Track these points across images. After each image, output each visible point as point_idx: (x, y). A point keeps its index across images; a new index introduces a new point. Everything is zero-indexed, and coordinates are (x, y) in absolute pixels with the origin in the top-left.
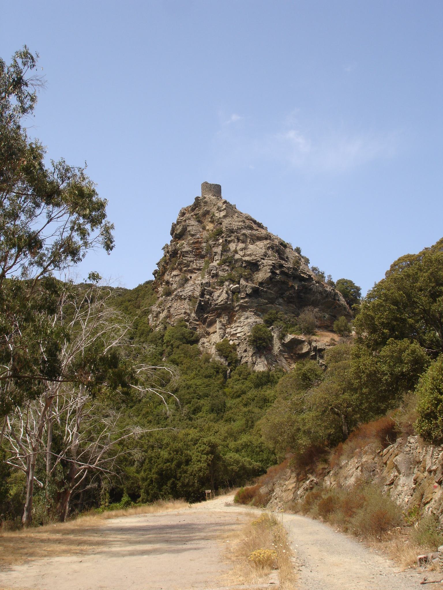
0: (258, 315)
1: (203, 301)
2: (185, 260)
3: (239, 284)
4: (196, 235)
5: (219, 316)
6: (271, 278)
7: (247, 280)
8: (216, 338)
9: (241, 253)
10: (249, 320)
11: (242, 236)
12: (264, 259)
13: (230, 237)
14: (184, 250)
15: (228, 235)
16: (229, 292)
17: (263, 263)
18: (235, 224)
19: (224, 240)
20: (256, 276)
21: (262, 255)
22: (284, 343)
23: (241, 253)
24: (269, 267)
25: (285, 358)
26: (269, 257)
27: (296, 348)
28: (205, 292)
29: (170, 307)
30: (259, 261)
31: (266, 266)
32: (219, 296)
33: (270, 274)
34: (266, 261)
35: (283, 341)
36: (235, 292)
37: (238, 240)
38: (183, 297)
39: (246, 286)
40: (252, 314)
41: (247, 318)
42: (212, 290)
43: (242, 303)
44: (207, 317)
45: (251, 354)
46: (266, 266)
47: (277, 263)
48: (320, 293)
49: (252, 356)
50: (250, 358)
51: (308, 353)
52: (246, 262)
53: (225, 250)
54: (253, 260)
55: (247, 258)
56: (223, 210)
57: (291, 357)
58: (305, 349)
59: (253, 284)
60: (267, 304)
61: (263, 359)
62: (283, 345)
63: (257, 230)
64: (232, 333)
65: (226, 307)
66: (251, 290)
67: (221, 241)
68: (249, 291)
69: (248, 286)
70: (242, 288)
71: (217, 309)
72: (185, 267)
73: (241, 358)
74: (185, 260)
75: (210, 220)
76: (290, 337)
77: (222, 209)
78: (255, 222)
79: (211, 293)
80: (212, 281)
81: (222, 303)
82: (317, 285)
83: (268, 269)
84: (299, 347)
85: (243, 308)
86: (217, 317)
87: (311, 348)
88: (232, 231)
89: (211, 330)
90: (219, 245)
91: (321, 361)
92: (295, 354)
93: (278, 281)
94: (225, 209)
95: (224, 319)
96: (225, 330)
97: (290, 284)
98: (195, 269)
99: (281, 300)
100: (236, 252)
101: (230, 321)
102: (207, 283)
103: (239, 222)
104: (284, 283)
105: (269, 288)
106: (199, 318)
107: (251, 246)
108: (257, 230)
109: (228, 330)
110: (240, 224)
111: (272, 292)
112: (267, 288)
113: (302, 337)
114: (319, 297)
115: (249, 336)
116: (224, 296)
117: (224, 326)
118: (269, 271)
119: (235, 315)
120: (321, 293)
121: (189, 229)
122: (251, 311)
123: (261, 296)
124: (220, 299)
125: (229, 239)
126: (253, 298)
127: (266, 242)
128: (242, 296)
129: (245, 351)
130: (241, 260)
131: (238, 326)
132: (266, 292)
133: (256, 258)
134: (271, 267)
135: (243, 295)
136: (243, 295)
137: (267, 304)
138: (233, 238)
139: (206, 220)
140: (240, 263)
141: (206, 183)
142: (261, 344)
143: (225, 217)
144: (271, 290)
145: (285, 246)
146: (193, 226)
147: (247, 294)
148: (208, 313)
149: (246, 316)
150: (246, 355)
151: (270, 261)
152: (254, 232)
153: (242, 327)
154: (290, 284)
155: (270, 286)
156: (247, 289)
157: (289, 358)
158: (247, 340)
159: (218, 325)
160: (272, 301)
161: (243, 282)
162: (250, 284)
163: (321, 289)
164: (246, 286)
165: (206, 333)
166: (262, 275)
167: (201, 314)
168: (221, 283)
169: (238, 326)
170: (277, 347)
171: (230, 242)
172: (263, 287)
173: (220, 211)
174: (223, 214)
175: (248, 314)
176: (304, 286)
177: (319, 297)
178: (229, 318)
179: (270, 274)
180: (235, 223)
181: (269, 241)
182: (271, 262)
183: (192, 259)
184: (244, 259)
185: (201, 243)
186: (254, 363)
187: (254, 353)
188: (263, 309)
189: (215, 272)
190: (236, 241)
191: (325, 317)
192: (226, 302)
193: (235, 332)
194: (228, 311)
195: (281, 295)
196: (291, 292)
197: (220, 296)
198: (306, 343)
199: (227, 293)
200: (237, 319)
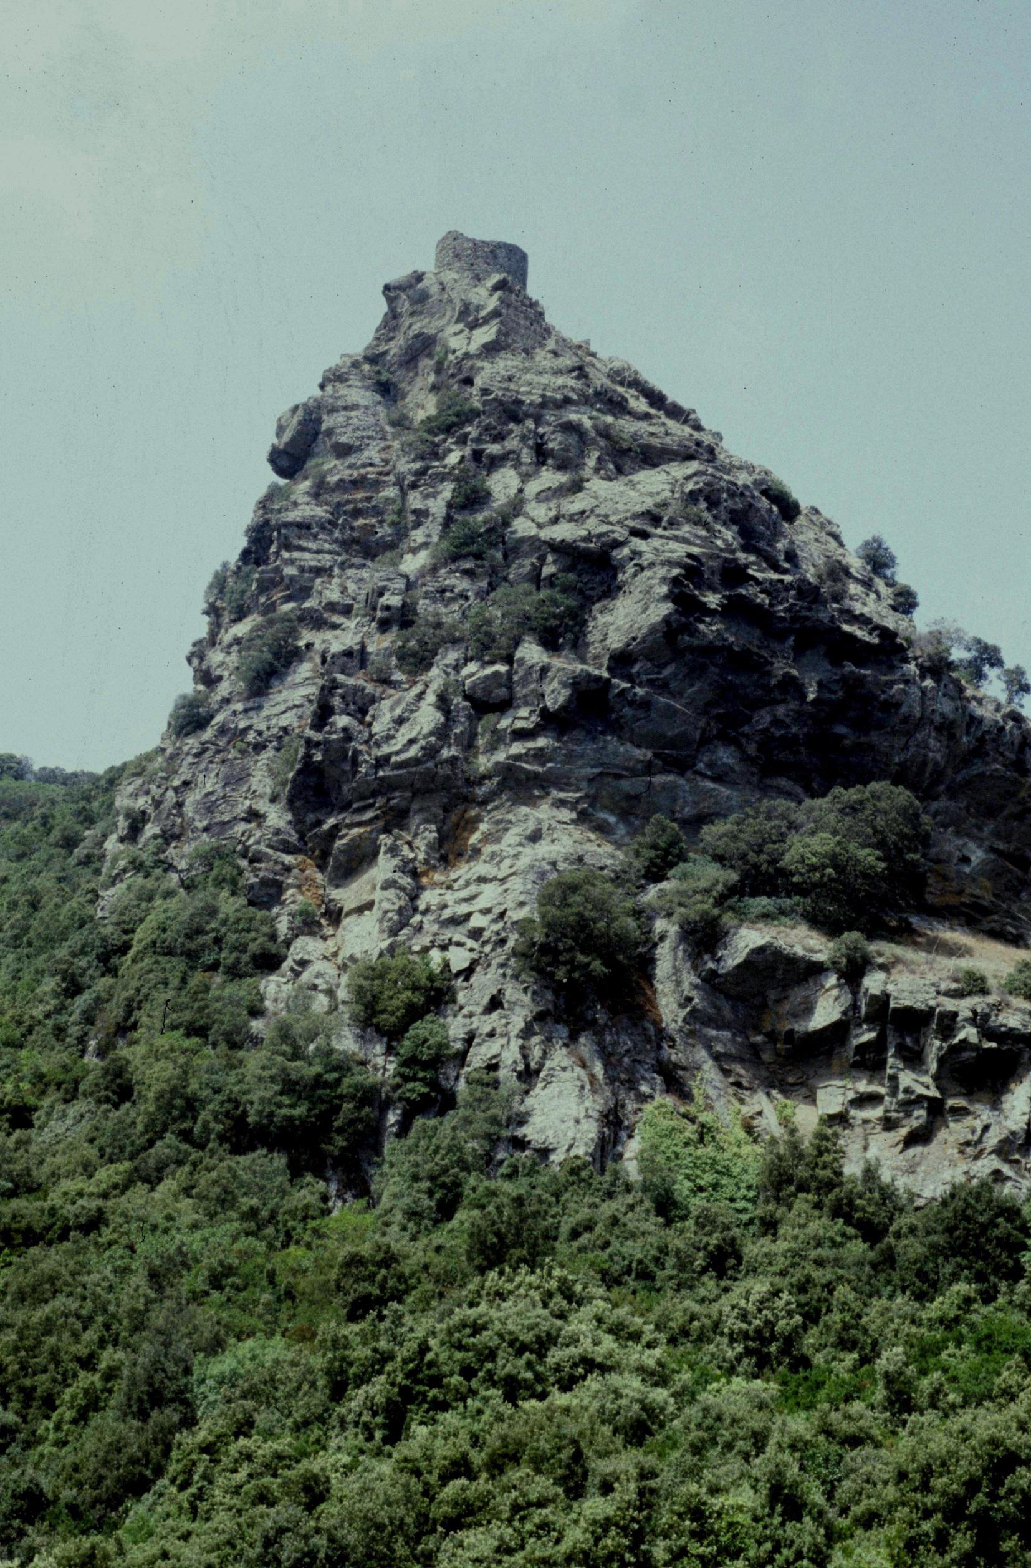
0: (602, 829)
1: (318, 744)
2: (292, 562)
3: (509, 659)
4: (359, 449)
5: (395, 820)
6: (669, 630)
7: (550, 643)
8: (362, 937)
9: (541, 512)
10: (544, 849)
11: (559, 437)
12: (644, 535)
13: (499, 438)
14: (293, 516)
15: (488, 428)
16: (458, 700)
17: (636, 554)
18: (537, 379)
19: (468, 451)
20: (602, 619)
21: (636, 516)
22: (713, 973)
23: (541, 512)
24: (662, 572)
25: (717, 1057)
26: (672, 523)
27: (778, 1001)
28: (336, 701)
29: (186, 784)
30: (618, 544)
31: (652, 565)
32: (400, 721)
33: (667, 608)
34: (655, 543)
35: (711, 965)
36: (487, 703)
37: (541, 454)
38: (251, 737)
39: (544, 670)
40: (566, 814)
41: (535, 837)
42: (370, 688)
43: (518, 757)
44: (336, 827)
45: (518, 1023)
46: (652, 565)
47: (711, 557)
48: (939, 729)
49: (527, 1033)
50: (515, 1044)
51: (838, 1031)
52: (560, 548)
53: (472, 498)
54: (588, 538)
55: (563, 532)
56: (486, 321)
57: (752, 1056)
58: (826, 1011)
59: (583, 661)
60: (648, 769)
61: (586, 1045)
62: (711, 981)
63: (647, 416)
64: (446, 914)
65: (432, 776)
66: (566, 693)
67: (453, 459)
68: (556, 695)
69: (550, 674)
70: (524, 681)
71: (385, 787)
72: (288, 599)
73: (469, 1040)
74: (292, 562)
75: (432, 378)
76: (747, 939)
77: (483, 313)
78: (637, 384)
79: (362, 708)
80: (380, 644)
81: (413, 751)
82: (929, 683)
83: (656, 582)
84: (798, 994)
85: (519, 784)
86: (387, 830)
87: (855, 1006)
88: (512, 412)
89: (347, 896)
90: (443, 477)
91: (906, 1079)
92: (772, 1036)
93: (710, 650)
94: (496, 314)
95: (423, 838)
96: (414, 898)
97: (781, 667)
98: (332, 607)
99: (725, 756)
100: (516, 507)
101: (449, 850)
102: (348, 653)
103: (558, 372)
104: (745, 662)
105: (662, 686)
106: (302, 837)
107: (597, 485)
108: (647, 416)
109: (429, 897)
110: (560, 381)
111: (681, 707)
112: (651, 683)
113: (804, 941)
114: (936, 750)
115: (522, 926)
116: (427, 717)
117: (415, 874)
118: (664, 589)
119: (478, 819)
120: (947, 728)
121: (328, 422)
122: (561, 803)
123: (616, 727)
124: (404, 734)
125: (494, 449)
126: (578, 734)
127: (678, 470)
128: (519, 724)
129: (495, 1004)
130: (534, 542)
131: (482, 880)
132: (645, 705)
133: (604, 528)
134: (676, 571)
135: (524, 717)
136: (524, 717)
137: (648, 769)
138: (512, 443)
139: (419, 382)
140: (526, 564)
141: (455, 236)
142: (585, 977)
143: (491, 350)
144: (672, 695)
145: (789, 509)
146: (355, 407)
147: (544, 713)
148: (345, 807)
149: (531, 826)
150: (491, 1023)
151: (673, 545)
152: (627, 426)
153: (503, 880)
154: (781, 667)
155: (667, 671)
156: (547, 688)
157: (741, 1060)
158: (511, 944)
159: (384, 868)
160: (676, 757)
161: (531, 652)
162: (564, 664)
163: (946, 707)
164: (544, 670)
165: (328, 913)
166: (628, 616)
167: (311, 817)
168: (418, 661)
169: (482, 880)
170: (672, 988)
171: (494, 463)
172: (630, 678)
173: (473, 326)
174: (485, 335)
175: (543, 813)
176: (853, 684)
177: (936, 750)
178: (442, 840)
179: (667, 608)
180: (536, 377)
181: (694, 466)
182: (679, 551)
183: (326, 560)
184: (545, 534)
185: (377, 485)
186: (528, 1075)
187: (540, 1017)
188: (629, 797)
189: (395, 601)
190: (527, 456)
191: (966, 860)
192: (431, 752)
193: (463, 909)
194: (443, 800)
195: (728, 730)
196: (781, 710)
197: (406, 722)
198: (832, 980)
199: (443, 702)
200: (487, 839)
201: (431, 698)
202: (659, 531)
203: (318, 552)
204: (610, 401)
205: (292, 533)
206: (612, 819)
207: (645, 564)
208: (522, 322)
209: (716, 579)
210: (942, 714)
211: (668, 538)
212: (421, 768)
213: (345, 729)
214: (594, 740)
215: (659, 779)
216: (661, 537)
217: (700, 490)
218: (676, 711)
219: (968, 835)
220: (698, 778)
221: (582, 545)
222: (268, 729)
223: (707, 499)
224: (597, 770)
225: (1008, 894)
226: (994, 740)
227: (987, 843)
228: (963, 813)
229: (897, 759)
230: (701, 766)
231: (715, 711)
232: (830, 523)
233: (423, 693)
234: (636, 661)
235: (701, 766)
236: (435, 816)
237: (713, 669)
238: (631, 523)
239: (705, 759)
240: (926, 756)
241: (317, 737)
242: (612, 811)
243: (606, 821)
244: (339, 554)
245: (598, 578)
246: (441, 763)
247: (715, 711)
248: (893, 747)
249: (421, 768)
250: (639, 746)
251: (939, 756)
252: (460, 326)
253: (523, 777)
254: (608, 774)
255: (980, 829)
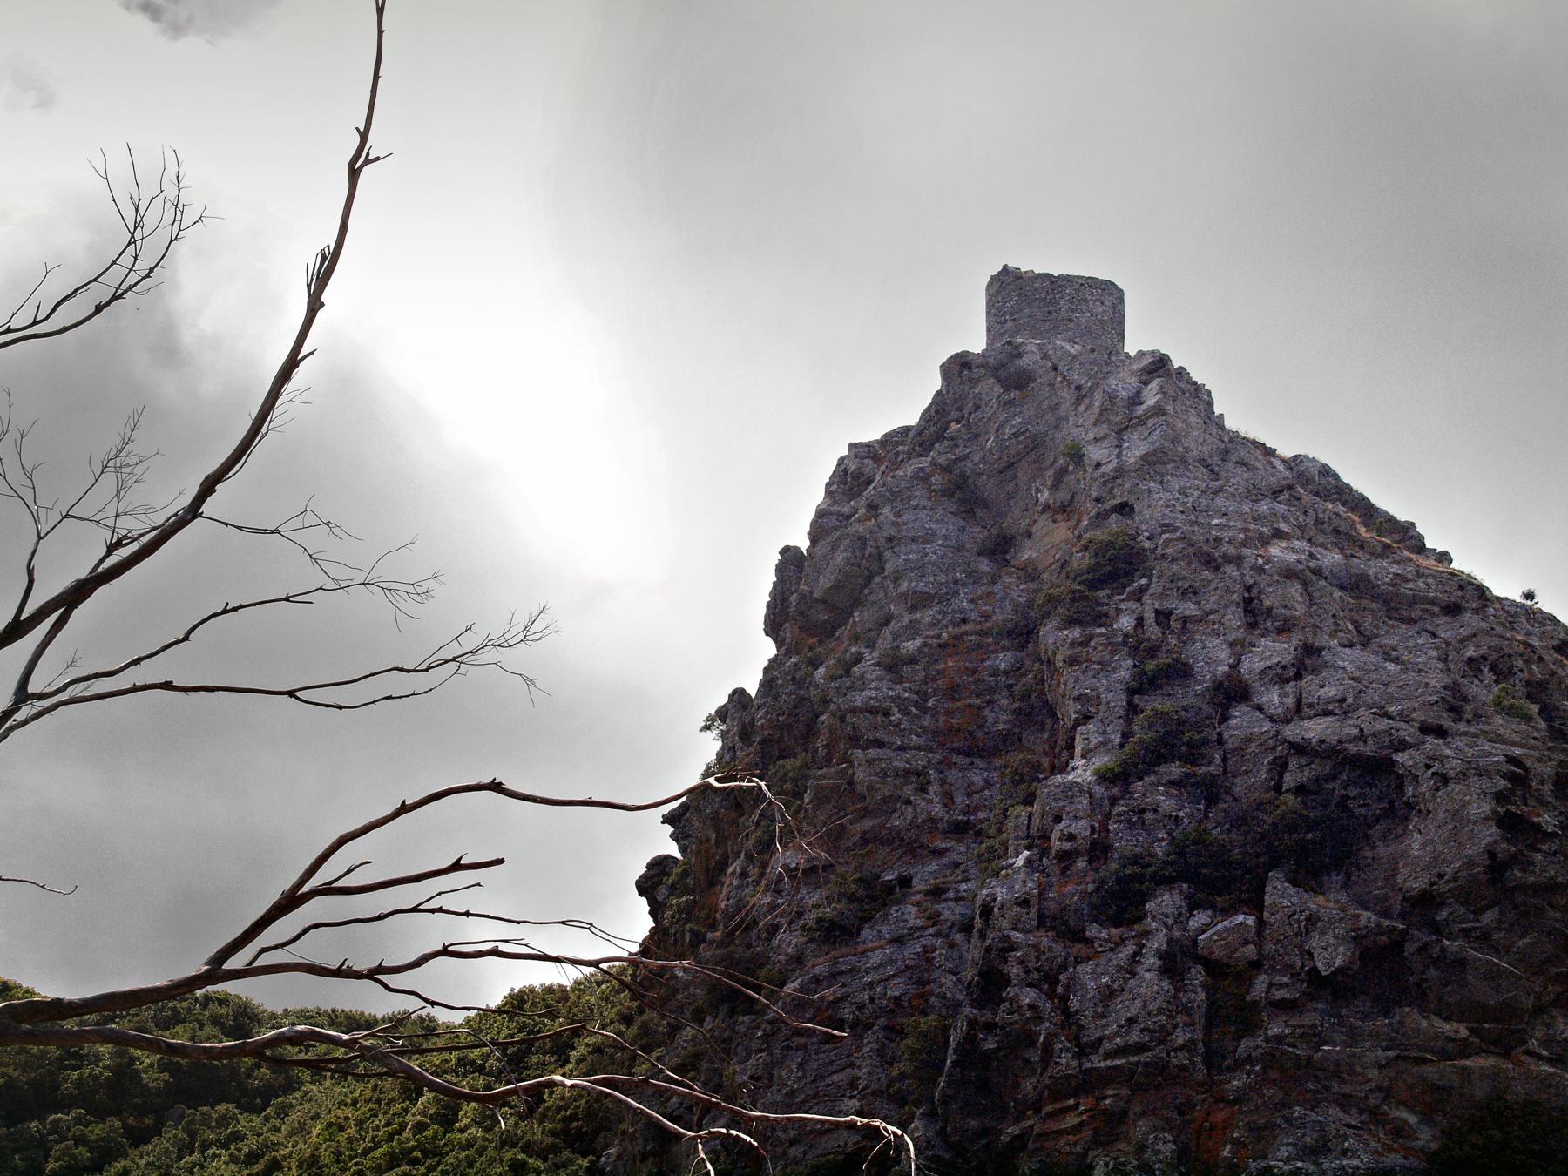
6: (1497, 866)
54: (1362, 737)
60: (1464, 1050)
100: (1232, 692)
105: (1483, 938)
123: (1420, 998)
144: (1495, 950)
155: (1488, 918)
172: (1436, 929)
190: (1234, 618)
201: (1151, 960)
202: (1462, 727)
203: (902, 748)
204: (1336, 531)
205: (863, 721)
206: (1413, 1119)
207: (1452, 773)
208: (1193, 419)
209: (1547, 788)
211: (1475, 736)
212: (1145, 1057)
213: (1032, 1007)
214: (1386, 1013)
215: (1475, 1062)
216: (1465, 734)
217: (1484, 658)
218: (1501, 972)
220: (1531, 1060)
221: (1352, 749)
222: (872, 1000)
223: (1493, 668)
224: (1391, 1054)
230: (1533, 1044)
231: (1553, 970)
233: (1137, 953)
234: (1443, 904)
235: (1533, 1044)
236: (1167, 1120)
237: (1551, 913)
238: (1420, 716)
239: (1538, 1034)
241: (985, 1016)
242: (1412, 1110)
243: (1405, 1121)
244: (931, 750)
245: (1375, 792)
246: (1175, 1050)
247: (1553, 970)
249: (1145, 1057)
250: (1448, 1019)
252: (1103, 429)
254: (1405, 1058)
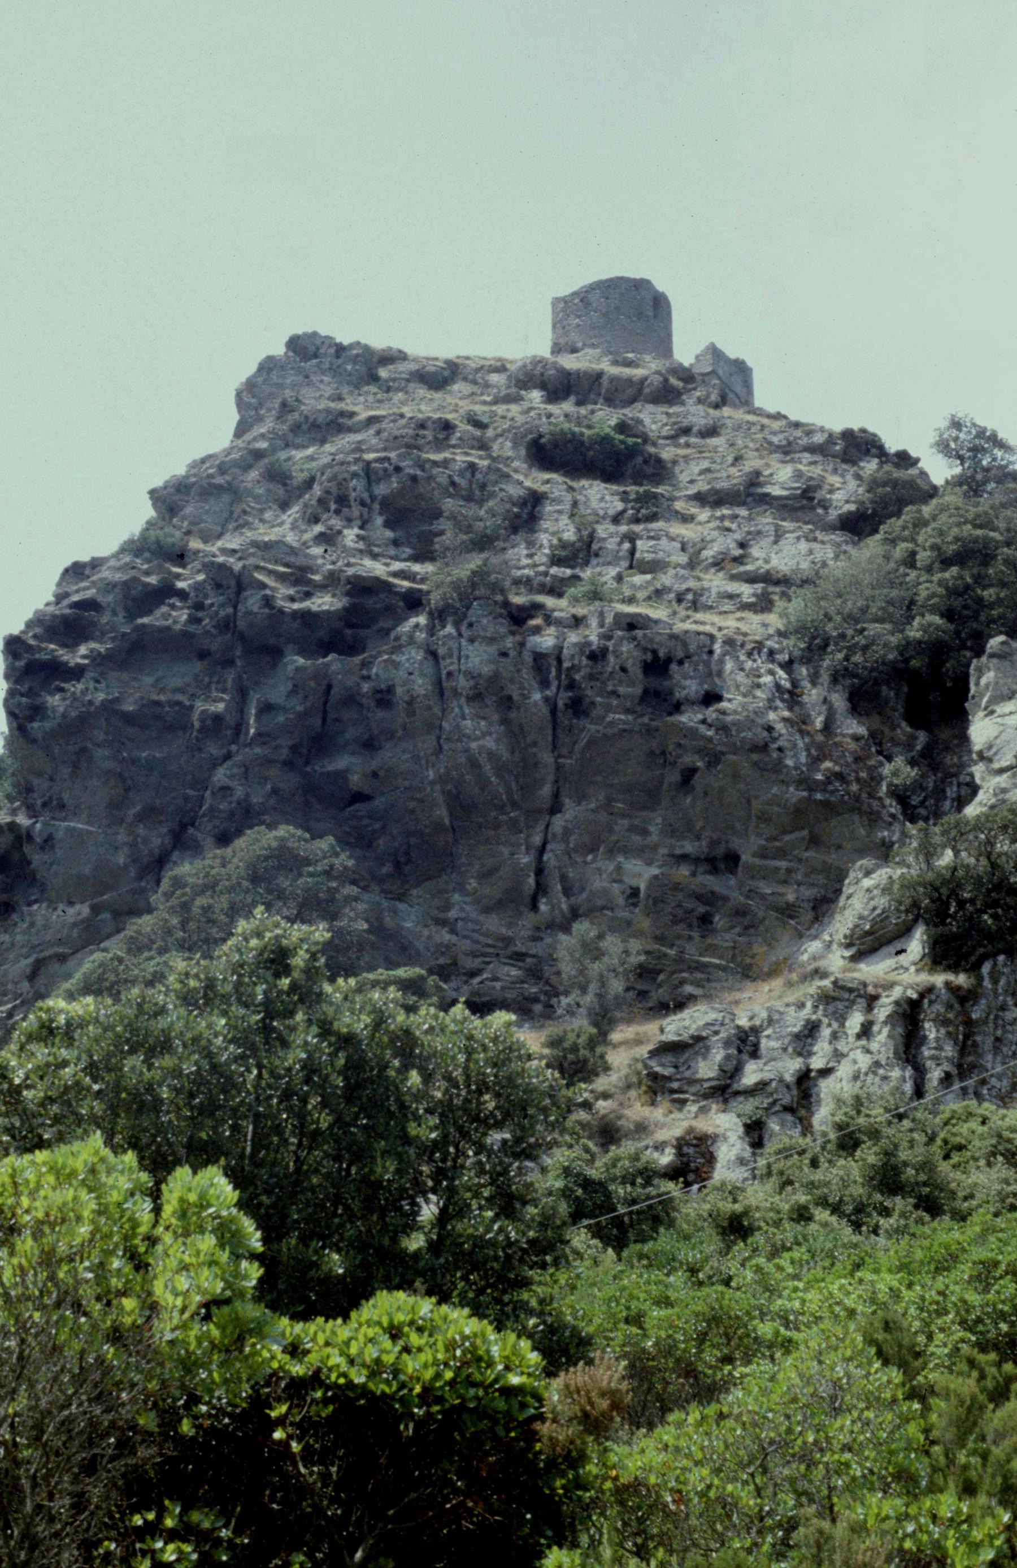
48: (476, 697)
210: (469, 674)
219: (625, 851)
225: (679, 928)
226: (591, 677)
227: (663, 851)
228: (603, 816)
229: (431, 774)
232: (996, 441)
240: (467, 750)
248: (416, 759)
251: (489, 743)
253: (618, 1015)
255: (645, 832)
